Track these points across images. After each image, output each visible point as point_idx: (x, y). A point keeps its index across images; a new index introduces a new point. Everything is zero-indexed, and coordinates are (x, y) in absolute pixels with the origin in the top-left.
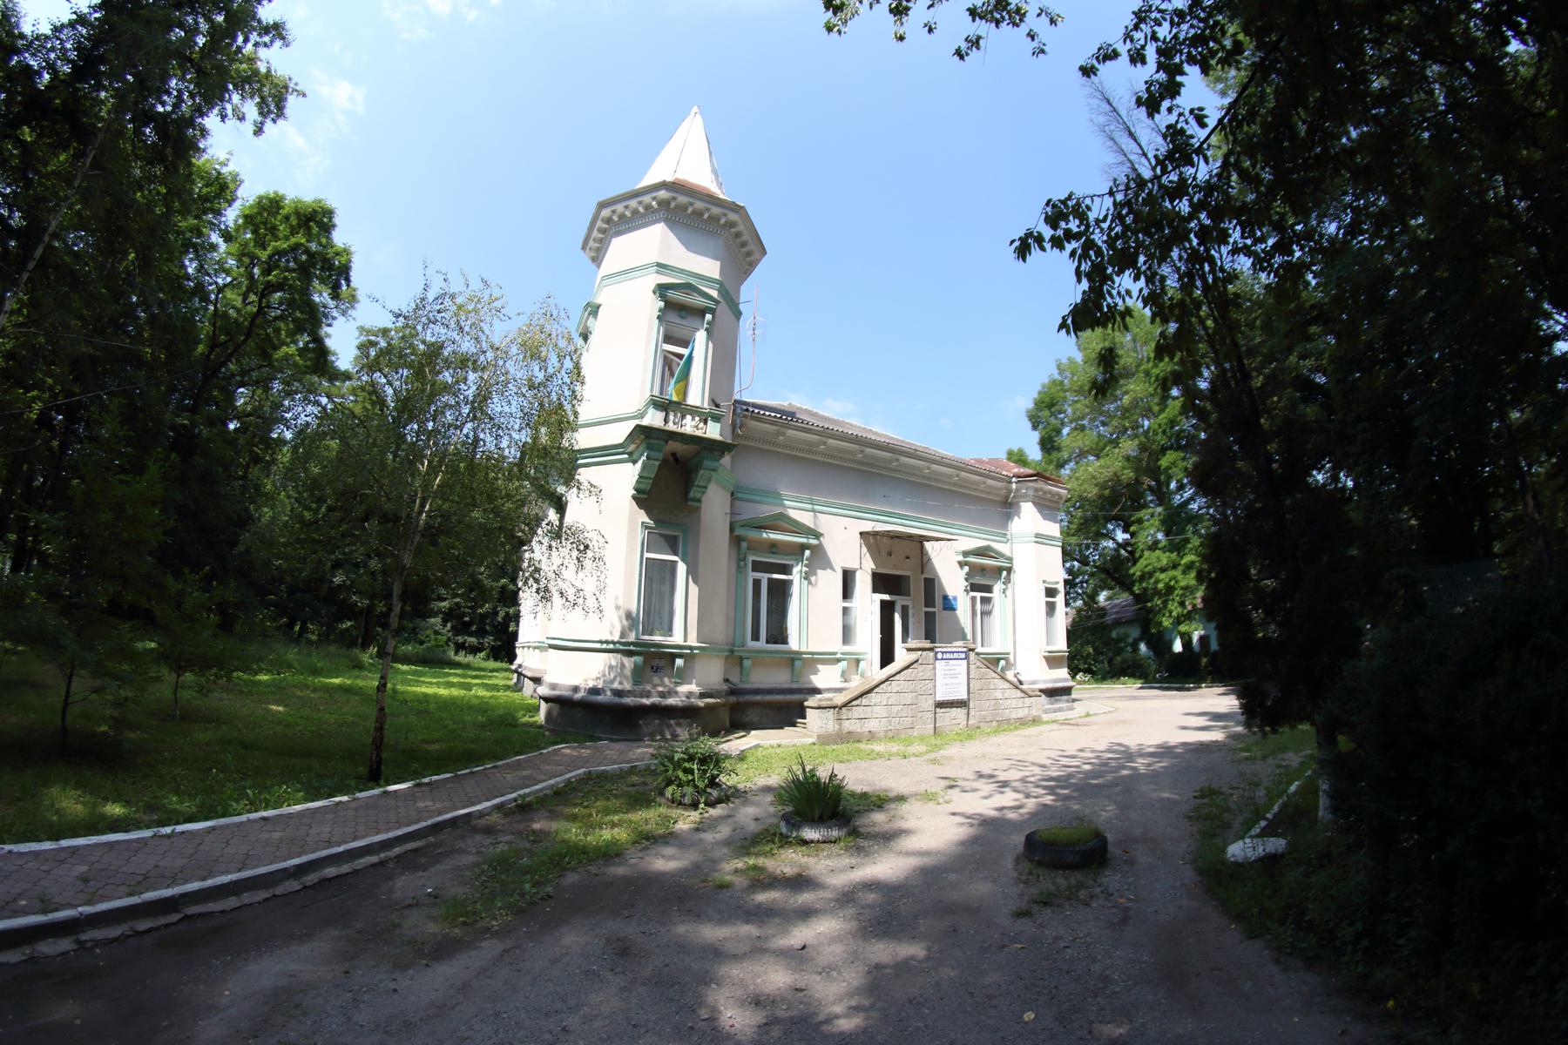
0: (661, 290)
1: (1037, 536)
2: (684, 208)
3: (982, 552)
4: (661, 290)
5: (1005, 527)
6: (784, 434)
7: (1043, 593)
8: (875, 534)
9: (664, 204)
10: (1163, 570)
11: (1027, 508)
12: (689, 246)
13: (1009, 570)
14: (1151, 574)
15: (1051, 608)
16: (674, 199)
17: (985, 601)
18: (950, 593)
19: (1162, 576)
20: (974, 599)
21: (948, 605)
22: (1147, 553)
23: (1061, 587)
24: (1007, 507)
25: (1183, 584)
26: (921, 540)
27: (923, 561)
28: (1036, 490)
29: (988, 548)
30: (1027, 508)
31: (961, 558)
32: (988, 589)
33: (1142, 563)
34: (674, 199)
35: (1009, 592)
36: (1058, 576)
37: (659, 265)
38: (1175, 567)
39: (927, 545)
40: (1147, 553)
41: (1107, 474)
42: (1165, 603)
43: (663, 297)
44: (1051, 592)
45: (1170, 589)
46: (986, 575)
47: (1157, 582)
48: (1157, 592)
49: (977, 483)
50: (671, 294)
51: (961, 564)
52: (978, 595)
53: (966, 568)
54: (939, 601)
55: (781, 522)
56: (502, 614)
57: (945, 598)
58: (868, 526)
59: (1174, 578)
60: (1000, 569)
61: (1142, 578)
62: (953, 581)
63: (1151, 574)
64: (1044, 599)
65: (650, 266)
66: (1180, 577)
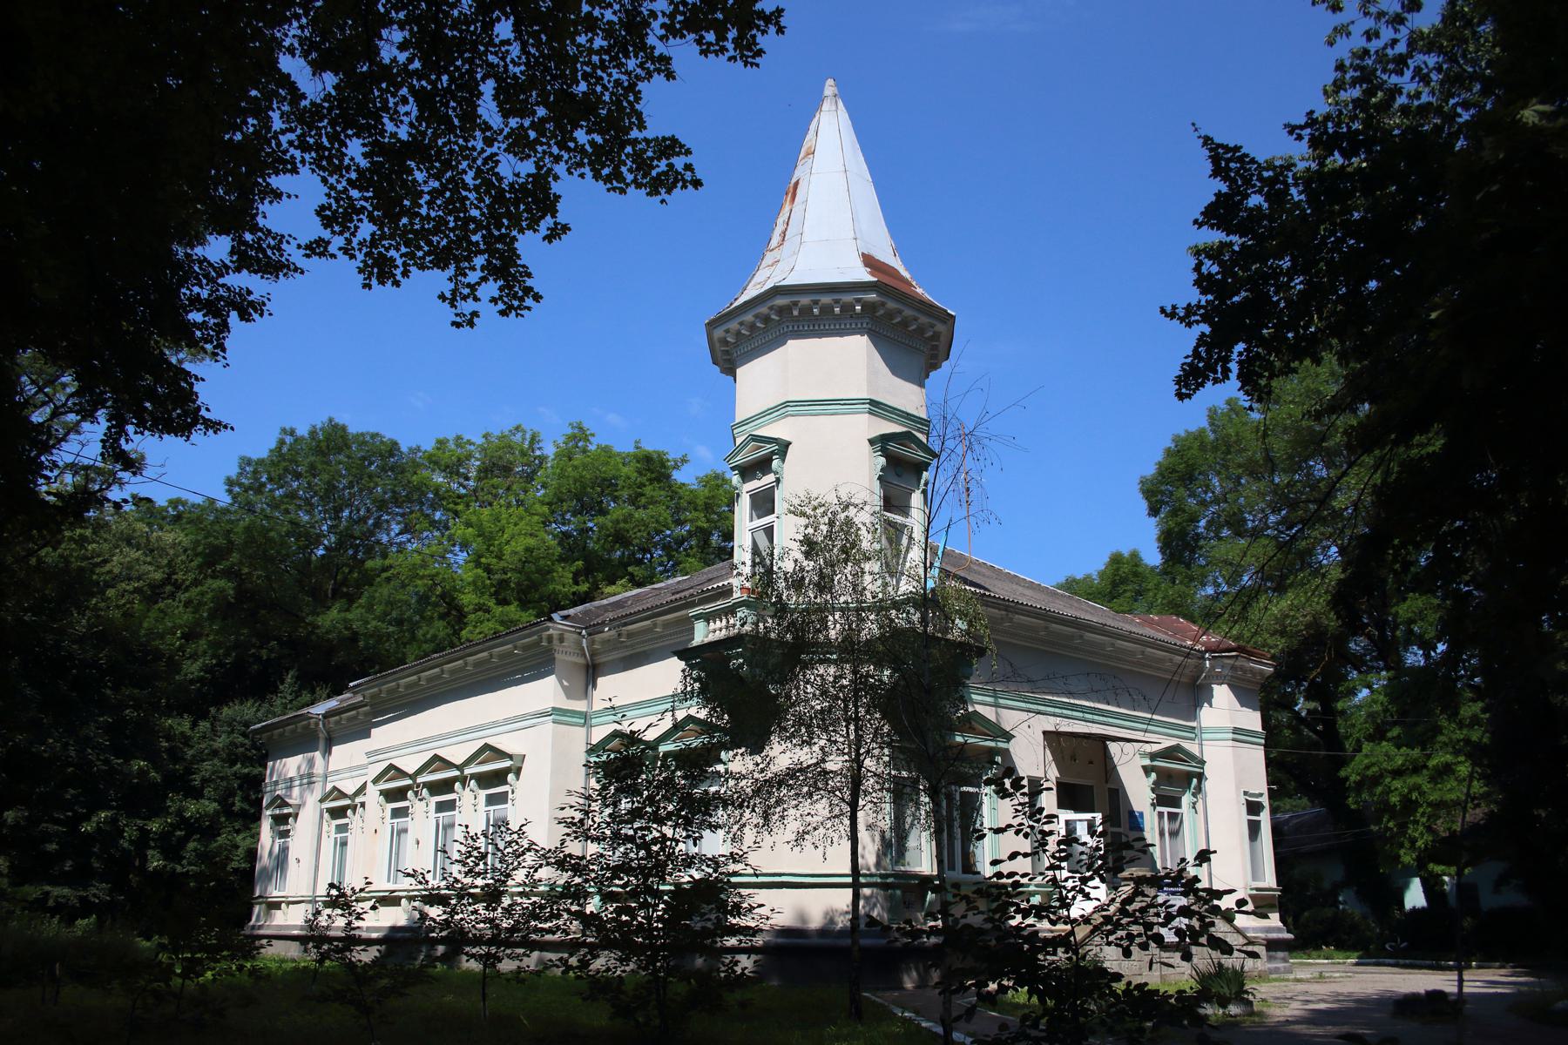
0: (881, 443)
1: (1236, 731)
2: (890, 315)
3: (1171, 753)
4: (881, 443)
5: (1193, 716)
6: (1011, 620)
7: (1244, 809)
8: (1058, 734)
9: (868, 307)
10: (1398, 773)
11: (1222, 694)
12: (896, 371)
13: (1201, 777)
14: (1376, 780)
15: (1254, 829)
16: (883, 304)
17: (1173, 817)
18: (1137, 808)
19: (1397, 784)
20: (1161, 815)
21: (1135, 822)
22: (1367, 747)
23: (1265, 800)
24: (1197, 695)
25: (1434, 797)
26: (1104, 739)
27: (1108, 769)
28: (1233, 668)
29: (1177, 748)
30: (1222, 694)
31: (1147, 762)
32: (1176, 802)
33: (1360, 761)
34: (932, 326)
35: (1200, 806)
36: (1259, 784)
37: (873, 403)
38: (1417, 769)
39: (1113, 748)
40: (1367, 747)
41: (1302, 619)
42: (1403, 827)
43: (885, 453)
44: (1253, 808)
45: (1409, 806)
46: (1178, 778)
47: (1388, 791)
48: (1387, 808)
49: (1161, 660)
50: (893, 447)
51: (1147, 770)
52: (1165, 810)
53: (1154, 775)
54: (1124, 818)
55: (973, 723)
56: (130, 833)
57: (1132, 812)
58: (1050, 724)
59: (1417, 788)
60: (1189, 776)
61: (1359, 786)
62: (1139, 791)
63: (1376, 780)
64: (1245, 817)
65: (861, 401)
66: (1426, 787)
